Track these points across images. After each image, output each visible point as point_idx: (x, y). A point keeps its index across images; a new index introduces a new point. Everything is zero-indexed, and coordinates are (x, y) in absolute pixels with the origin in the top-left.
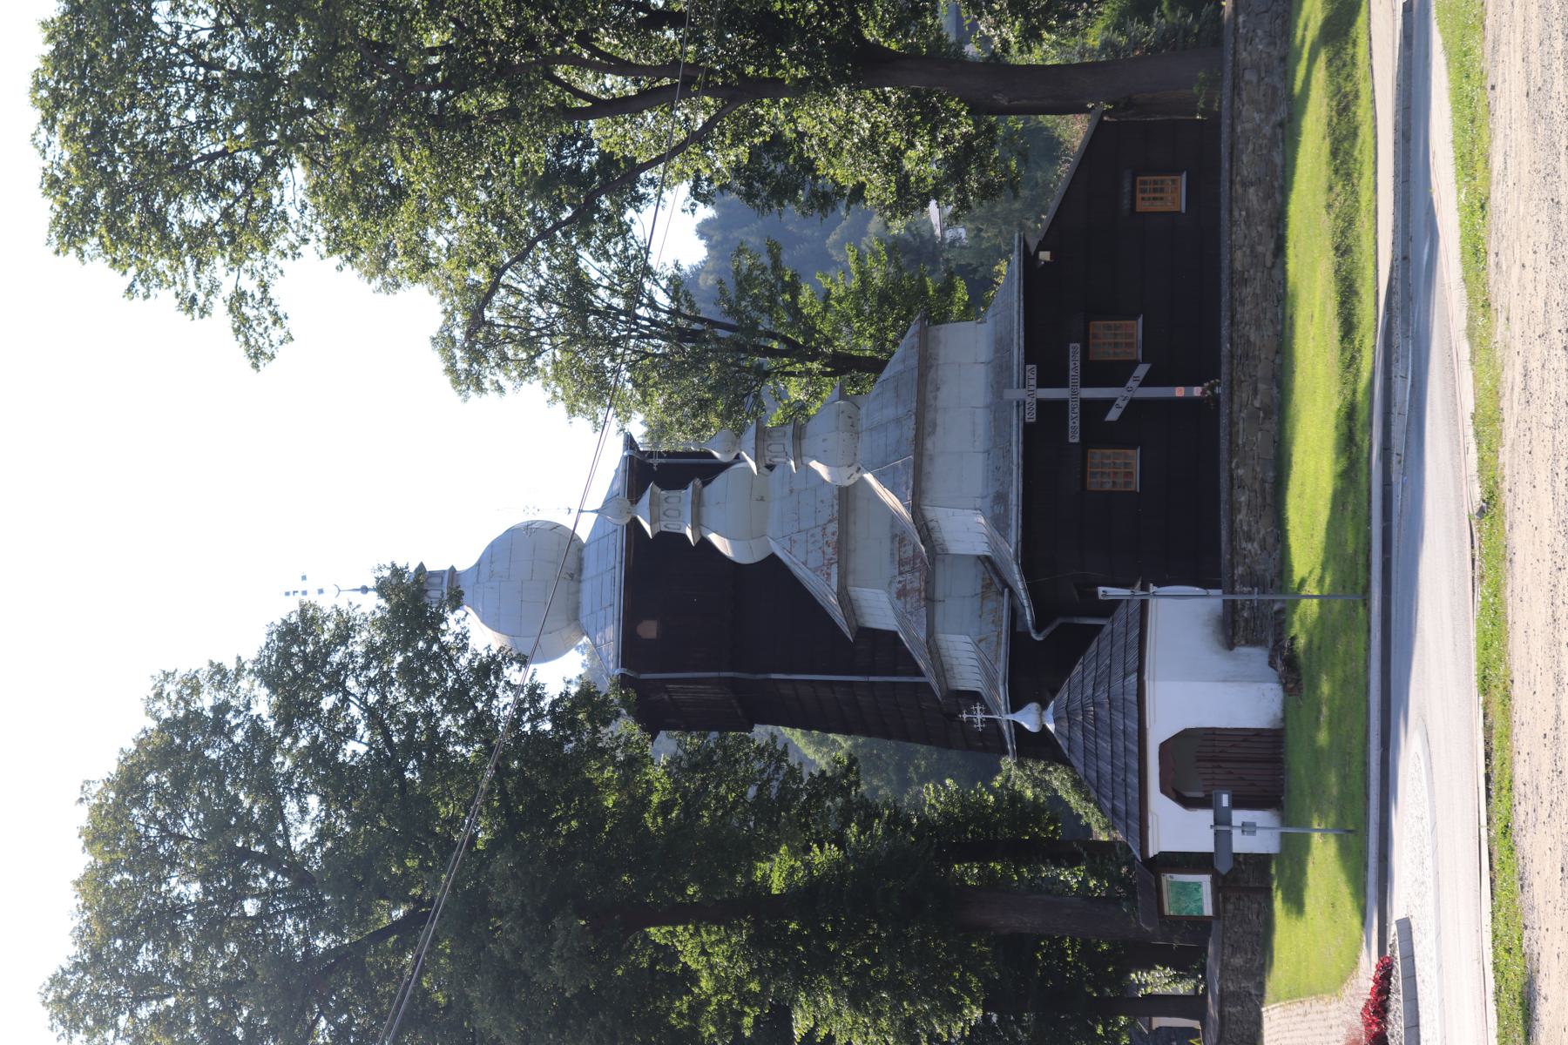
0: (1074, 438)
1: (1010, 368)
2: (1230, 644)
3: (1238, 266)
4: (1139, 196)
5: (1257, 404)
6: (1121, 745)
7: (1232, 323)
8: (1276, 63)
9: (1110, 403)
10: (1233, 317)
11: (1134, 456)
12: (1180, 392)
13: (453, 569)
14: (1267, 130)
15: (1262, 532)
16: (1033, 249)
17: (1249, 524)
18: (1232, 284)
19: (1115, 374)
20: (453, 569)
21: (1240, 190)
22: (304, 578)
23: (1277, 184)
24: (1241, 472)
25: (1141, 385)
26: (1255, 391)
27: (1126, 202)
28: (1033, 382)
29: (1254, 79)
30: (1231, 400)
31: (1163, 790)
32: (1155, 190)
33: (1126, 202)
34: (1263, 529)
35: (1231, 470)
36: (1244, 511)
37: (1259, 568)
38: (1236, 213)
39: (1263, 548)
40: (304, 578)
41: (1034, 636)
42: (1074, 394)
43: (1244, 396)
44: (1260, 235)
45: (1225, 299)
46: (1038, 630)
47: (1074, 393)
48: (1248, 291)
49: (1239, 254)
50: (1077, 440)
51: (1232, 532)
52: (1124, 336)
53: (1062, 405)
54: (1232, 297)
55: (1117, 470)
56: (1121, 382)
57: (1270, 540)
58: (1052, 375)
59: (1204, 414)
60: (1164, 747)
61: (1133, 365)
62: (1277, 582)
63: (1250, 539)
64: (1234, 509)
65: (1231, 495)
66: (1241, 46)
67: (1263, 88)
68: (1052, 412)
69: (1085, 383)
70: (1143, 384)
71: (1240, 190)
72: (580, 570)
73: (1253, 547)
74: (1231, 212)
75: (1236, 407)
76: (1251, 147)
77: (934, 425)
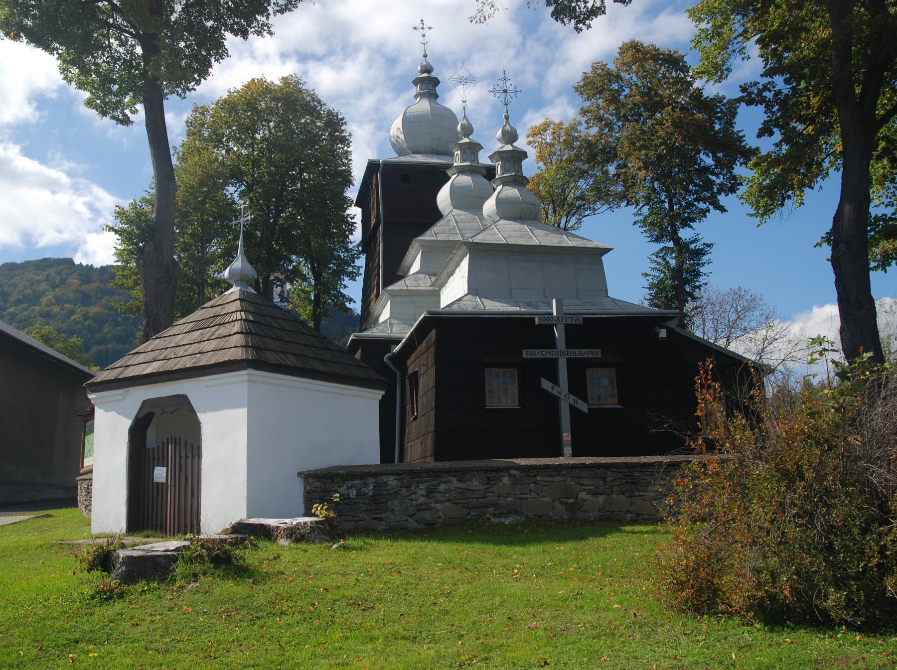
0: (526, 354)
2: (300, 474)
5: (582, 495)
9: (555, 381)
12: (566, 436)
19: (578, 387)
22: (430, 28)
23: (27, 513)
24: (506, 480)
25: (570, 405)
26: (596, 494)
28: (569, 322)
34: (443, 509)
39: (420, 508)
40: (430, 28)
41: (388, 355)
42: (562, 354)
47: (562, 353)
50: (525, 356)
52: (603, 388)
55: (502, 392)
56: (572, 390)
57: (428, 515)
61: (585, 399)
63: (430, 492)
69: (570, 361)
70: (572, 407)
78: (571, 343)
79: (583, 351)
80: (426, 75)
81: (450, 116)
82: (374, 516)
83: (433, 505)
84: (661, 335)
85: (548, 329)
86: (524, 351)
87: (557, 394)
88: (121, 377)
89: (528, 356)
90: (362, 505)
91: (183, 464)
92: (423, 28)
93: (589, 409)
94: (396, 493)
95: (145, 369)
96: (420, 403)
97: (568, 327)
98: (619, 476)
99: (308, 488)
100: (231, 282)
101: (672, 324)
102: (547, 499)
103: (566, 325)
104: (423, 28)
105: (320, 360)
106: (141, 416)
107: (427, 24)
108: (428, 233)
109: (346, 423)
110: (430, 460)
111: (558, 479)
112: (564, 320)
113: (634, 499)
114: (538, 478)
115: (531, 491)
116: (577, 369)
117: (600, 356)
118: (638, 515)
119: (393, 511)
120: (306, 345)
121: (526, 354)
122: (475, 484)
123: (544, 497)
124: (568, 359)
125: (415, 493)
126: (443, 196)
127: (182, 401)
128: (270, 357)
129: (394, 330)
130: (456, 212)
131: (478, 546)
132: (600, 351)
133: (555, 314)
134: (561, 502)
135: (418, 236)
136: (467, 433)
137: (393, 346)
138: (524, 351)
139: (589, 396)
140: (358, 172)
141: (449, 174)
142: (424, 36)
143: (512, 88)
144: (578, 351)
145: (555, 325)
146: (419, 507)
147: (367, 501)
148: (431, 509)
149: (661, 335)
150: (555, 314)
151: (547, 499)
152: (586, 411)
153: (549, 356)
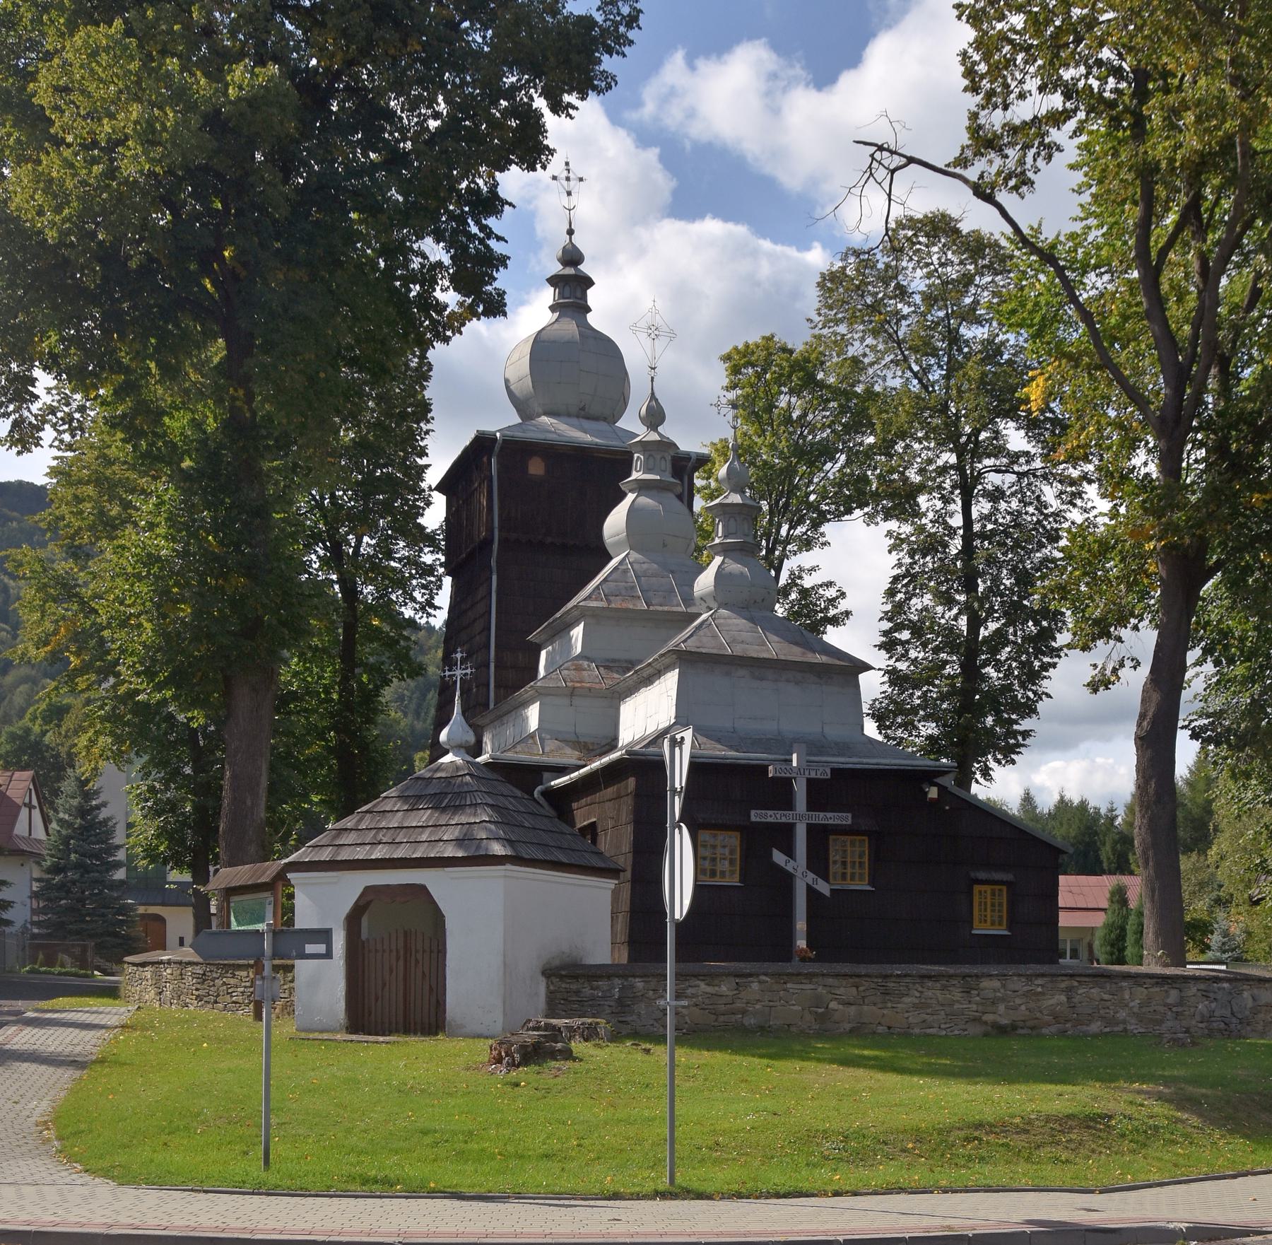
0: (755, 816)
1: (821, 755)
2: (549, 973)
3: (985, 983)
4: (988, 888)
5: (833, 1005)
6: (424, 837)
7: (923, 977)
8: (1184, 1023)
9: (789, 852)
10: (929, 977)
11: (735, 881)
12: (801, 925)
13: (589, 310)
14: (1122, 1014)
16: (939, 780)
17: (694, 996)
19: (818, 862)
20: (589, 310)
21: (1063, 985)
22: (581, 180)
24: (755, 986)
27: (982, 875)
28: (813, 775)
29: (1170, 1001)
30: (837, 976)
31: (367, 890)
32: (993, 905)
33: (982, 875)
35: (758, 975)
36: (709, 989)
37: (641, 1008)
38: (1039, 981)
40: (581, 180)
41: (539, 788)
42: (800, 817)
43: (842, 991)
44: (1015, 1009)
45: (951, 970)
46: (543, 793)
48: (957, 994)
49: (996, 984)
50: (753, 819)
52: (853, 870)
53: (789, 804)
54: (951, 976)
58: (820, 794)
59: (781, 949)
60: (421, 891)
61: (827, 880)
62: (625, 1030)
64: (710, 977)
66: (1202, 986)
67: (1162, 1009)
68: (780, 793)
69: (811, 829)
71: (1063, 985)
72: (588, 418)
74: (1043, 975)
75: (830, 981)
76: (1106, 997)
77: (762, 679)
78: (815, 803)
79: (829, 815)
84: (930, 796)
86: (753, 812)
87: (791, 870)
92: (568, 179)
97: (809, 781)
98: (873, 986)
101: (949, 781)
103: (808, 780)
106: (361, 903)
113: (885, 1012)
114: (789, 985)
115: (780, 999)
116: (818, 835)
118: (889, 1028)
119: (639, 1015)
121: (755, 816)
126: (616, 522)
128: (526, 852)
131: (718, 1055)
132: (850, 815)
133: (795, 764)
138: (753, 812)
142: (569, 194)
144: (822, 814)
149: (930, 796)
150: (795, 764)
152: (828, 894)
153: (784, 820)
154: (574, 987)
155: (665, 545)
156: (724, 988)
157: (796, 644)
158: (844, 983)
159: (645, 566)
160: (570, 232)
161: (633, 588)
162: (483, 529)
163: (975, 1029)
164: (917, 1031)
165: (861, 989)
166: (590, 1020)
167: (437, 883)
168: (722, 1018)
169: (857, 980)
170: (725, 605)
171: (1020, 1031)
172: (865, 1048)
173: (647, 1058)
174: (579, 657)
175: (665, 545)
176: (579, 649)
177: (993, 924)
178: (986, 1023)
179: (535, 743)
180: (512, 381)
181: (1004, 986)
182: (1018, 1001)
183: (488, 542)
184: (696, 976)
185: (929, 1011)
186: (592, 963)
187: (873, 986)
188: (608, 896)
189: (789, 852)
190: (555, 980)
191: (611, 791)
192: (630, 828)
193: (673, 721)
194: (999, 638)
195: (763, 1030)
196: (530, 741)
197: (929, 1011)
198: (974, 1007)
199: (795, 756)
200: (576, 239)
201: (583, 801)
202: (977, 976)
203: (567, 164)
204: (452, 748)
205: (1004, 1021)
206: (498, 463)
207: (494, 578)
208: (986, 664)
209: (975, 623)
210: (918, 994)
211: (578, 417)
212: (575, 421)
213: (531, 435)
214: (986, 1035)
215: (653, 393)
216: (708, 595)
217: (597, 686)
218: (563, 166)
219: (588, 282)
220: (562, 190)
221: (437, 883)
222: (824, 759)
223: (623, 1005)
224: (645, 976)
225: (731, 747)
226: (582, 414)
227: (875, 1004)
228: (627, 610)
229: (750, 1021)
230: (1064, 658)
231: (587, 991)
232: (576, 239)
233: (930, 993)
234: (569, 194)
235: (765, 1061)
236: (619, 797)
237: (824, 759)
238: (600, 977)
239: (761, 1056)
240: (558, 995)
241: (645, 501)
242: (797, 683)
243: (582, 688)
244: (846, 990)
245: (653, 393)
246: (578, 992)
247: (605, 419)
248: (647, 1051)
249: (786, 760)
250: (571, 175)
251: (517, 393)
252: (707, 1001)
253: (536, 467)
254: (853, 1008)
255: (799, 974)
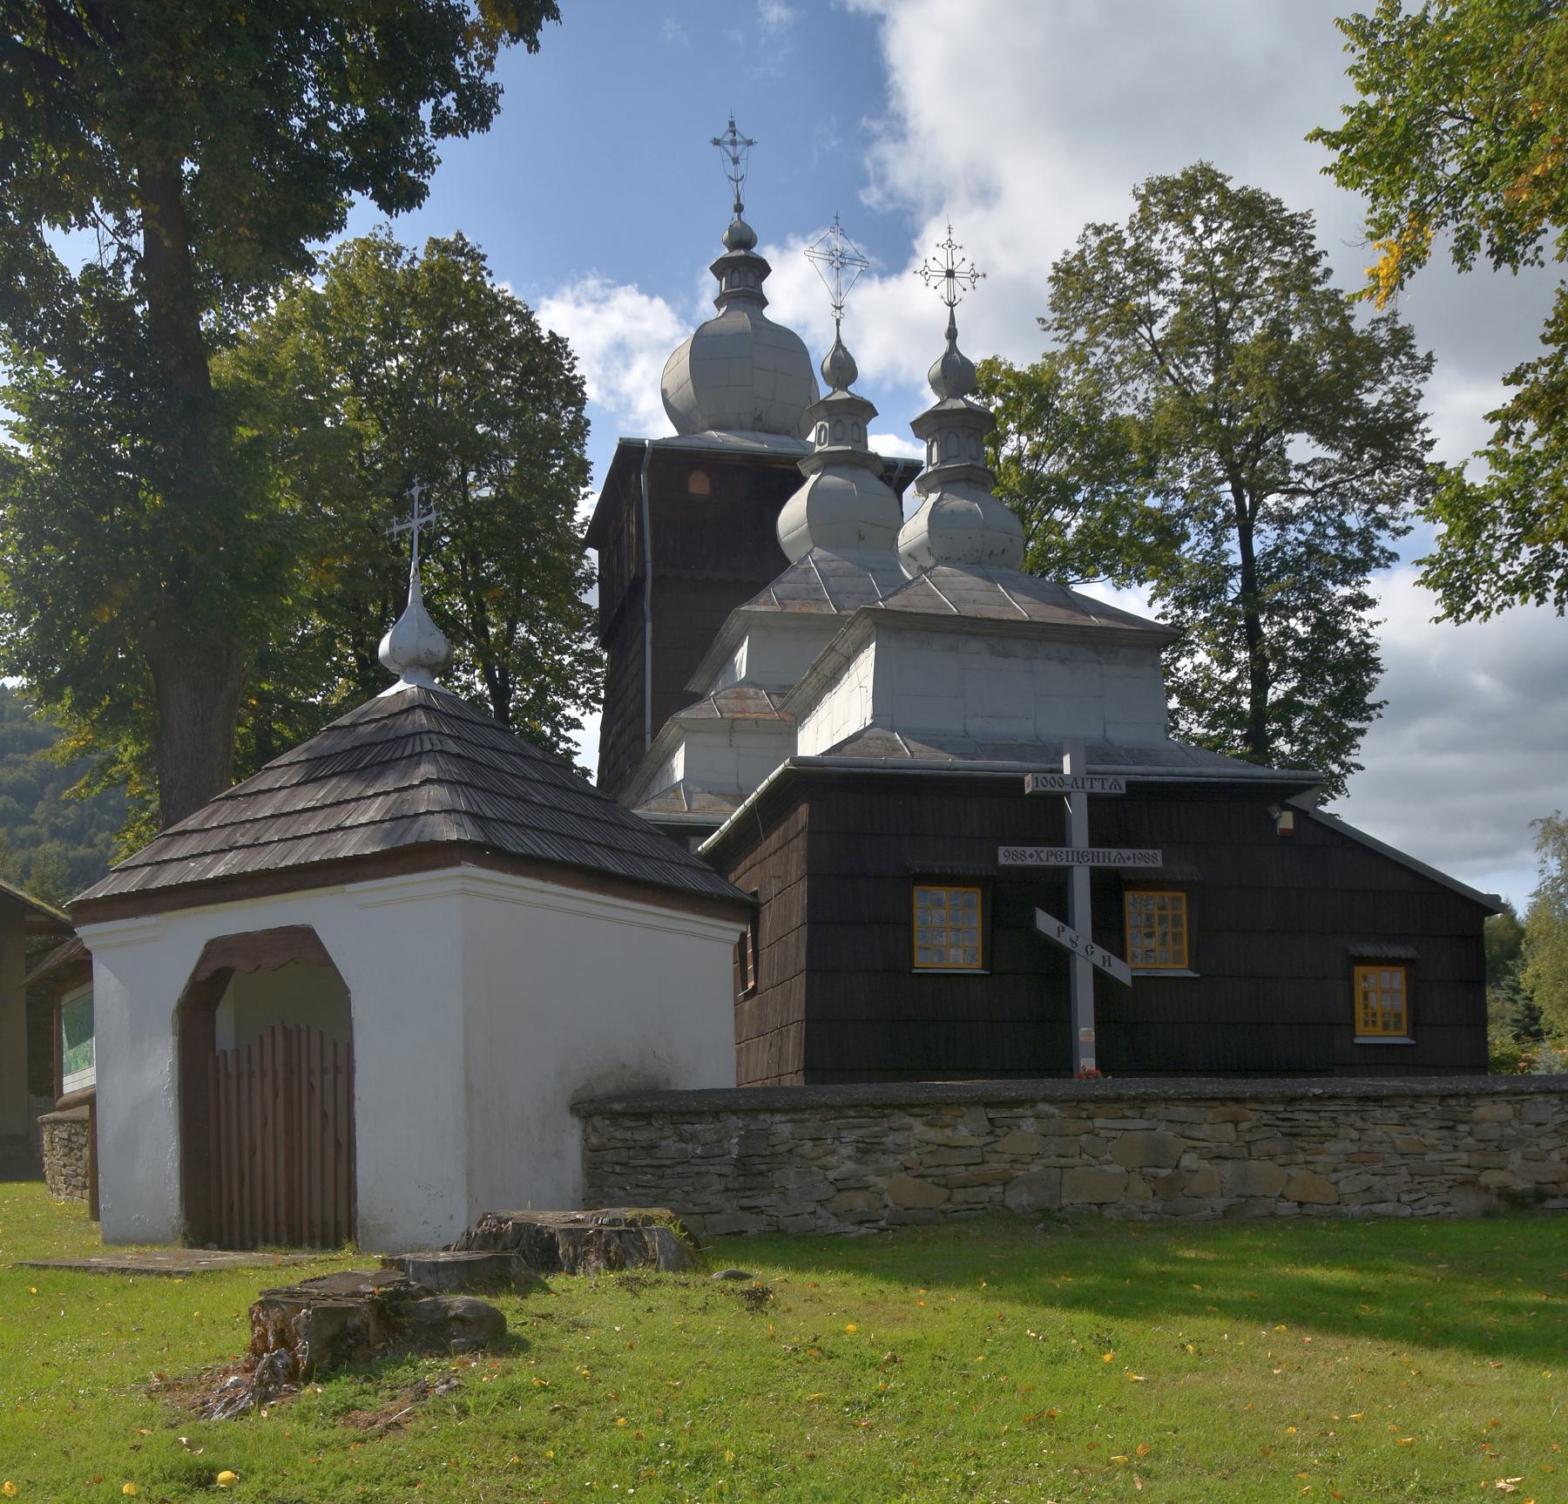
0: (1007, 856)
2: (587, 1108)
5: (1189, 1161)
7: (1364, 1099)
9: (1063, 913)
10: (1378, 1099)
12: (1086, 1033)
15: (882, 1182)
17: (900, 1149)
18: (1443, 1097)
19: (1109, 930)
22: (750, 143)
24: (1029, 1125)
28: (1097, 788)
30: (1196, 1100)
35: (1033, 1102)
36: (933, 1135)
39: (841, 1185)
40: (750, 143)
42: (1079, 857)
45: (1417, 1085)
49: (1503, 1110)
50: (1002, 860)
51: (883, 1108)
53: (1056, 834)
54: (1418, 1097)
57: (859, 1201)
60: (303, 939)
61: (1122, 956)
62: (754, 1225)
63: (865, 1150)
64: (932, 1109)
65: (974, 1102)
68: (1044, 820)
70: (1099, 975)
73: (842, 1162)
75: (1182, 1111)
77: (1006, 656)
79: (1126, 852)
80: (742, 252)
81: (788, 343)
82: (744, 1202)
83: (871, 1179)
85: (1052, 804)
86: (1002, 850)
87: (1068, 944)
88: (153, 886)
89: (1010, 862)
90: (715, 1179)
91: (317, 1084)
93: (1134, 978)
94: (790, 1151)
95: (210, 868)
96: (764, 956)
97: (1093, 800)
98: (1267, 1119)
99: (594, 1140)
100: (394, 669)
102: (1115, 1169)
104: (734, 143)
105: (611, 848)
106: (202, 977)
107: (744, 130)
108: (762, 597)
109: (680, 995)
110: (798, 1081)
111: (1143, 1124)
112: (1087, 784)
113: (1294, 1171)
114: (1099, 1122)
115: (1082, 1151)
117: (1159, 864)
118: (1301, 1204)
119: (784, 1191)
120: (579, 816)
122: (963, 1134)
123: (1109, 1163)
124: (1092, 869)
125: (834, 1152)
126: (793, 513)
127: (301, 943)
128: (511, 841)
129: (695, 805)
130: (819, 553)
132: (1159, 853)
133: (1067, 770)
134: (1144, 1177)
135: (741, 604)
136: (873, 1026)
137: (693, 840)
138: (1002, 850)
139: (1129, 950)
140: (600, 455)
141: (804, 472)
142: (736, 161)
143: (965, 267)
145: (1068, 795)
146: (840, 1185)
147: (725, 1170)
148: (867, 1188)
151: (1115, 1169)
152: (1128, 981)
153: (1053, 862)
154: (642, 1136)
155: (861, 538)
156: (964, 1131)
157: (1060, 605)
158: (1210, 1114)
159: (834, 565)
160: (739, 208)
161: (818, 590)
162: (633, 568)
163: (1470, 1202)
164: (1355, 1208)
165: (1244, 1126)
166: (630, 1213)
167: (321, 912)
168: (960, 1195)
169: (1234, 1107)
170: (946, 561)
171: (1552, 1203)
172: (1307, 1260)
173: (760, 1326)
174: (746, 682)
175: (861, 538)
176: (743, 674)
177: (1386, 1026)
178: (1487, 1189)
179: (679, 798)
180: (670, 392)
181: (1518, 1115)
182: (1546, 1144)
183: (639, 582)
184: (905, 1107)
185: (1378, 1167)
186: (681, 1088)
187: (1267, 1119)
188: (727, 955)
189: (1063, 913)
190: (598, 1121)
191: (775, 839)
192: (803, 887)
193: (869, 722)
194: (1288, 706)
195: (1048, 1217)
196: (672, 795)
197: (1378, 1167)
198: (1464, 1158)
199: (1067, 760)
200: (746, 217)
201: (741, 868)
202: (1468, 1095)
203: (732, 124)
204: (404, 668)
205: (1521, 1185)
206: (650, 479)
207: (649, 626)
208: (1277, 734)
209: (1262, 682)
210: (1355, 1135)
211: (753, 430)
212: (749, 434)
213: (693, 442)
214: (1488, 1214)
215: (839, 341)
216: (919, 547)
217: (767, 717)
218: (727, 127)
219: (763, 269)
220: (726, 156)
221: (340, 920)
222: (1112, 768)
223: (751, 1171)
224: (795, 1109)
225: (962, 755)
226: (759, 425)
227: (1271, 1157)
228: (809, 616)
229: (1020, 1199)
230: (1376, 721)
231: (671, 1146)
232: (746, 217)
233: (1378, 1132)
234: (736, 161)
235: (1084, 1319)
236: (787, 843)
237: (1112, 768)
238: (699, 1114)
239: (1074, 1301)
240: (610, 1156)
241: (831, 480)
242: (1061, 661)
243: (744, 719)
244: (1214, 1129)
245: (839, 341)
246: (650, 1148)
247: (788, 433)
248: (758, 1299)
249: (1052, 771)
250: (738, 138)
251: (676, 405)
252: (928, 1160)
253: (699, 485)
254: (1229, 1165)
255: (1119, 1099)
